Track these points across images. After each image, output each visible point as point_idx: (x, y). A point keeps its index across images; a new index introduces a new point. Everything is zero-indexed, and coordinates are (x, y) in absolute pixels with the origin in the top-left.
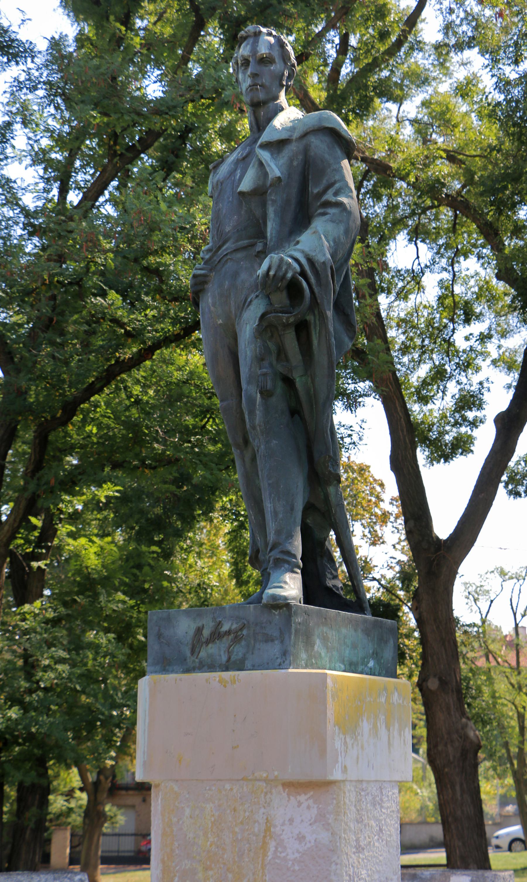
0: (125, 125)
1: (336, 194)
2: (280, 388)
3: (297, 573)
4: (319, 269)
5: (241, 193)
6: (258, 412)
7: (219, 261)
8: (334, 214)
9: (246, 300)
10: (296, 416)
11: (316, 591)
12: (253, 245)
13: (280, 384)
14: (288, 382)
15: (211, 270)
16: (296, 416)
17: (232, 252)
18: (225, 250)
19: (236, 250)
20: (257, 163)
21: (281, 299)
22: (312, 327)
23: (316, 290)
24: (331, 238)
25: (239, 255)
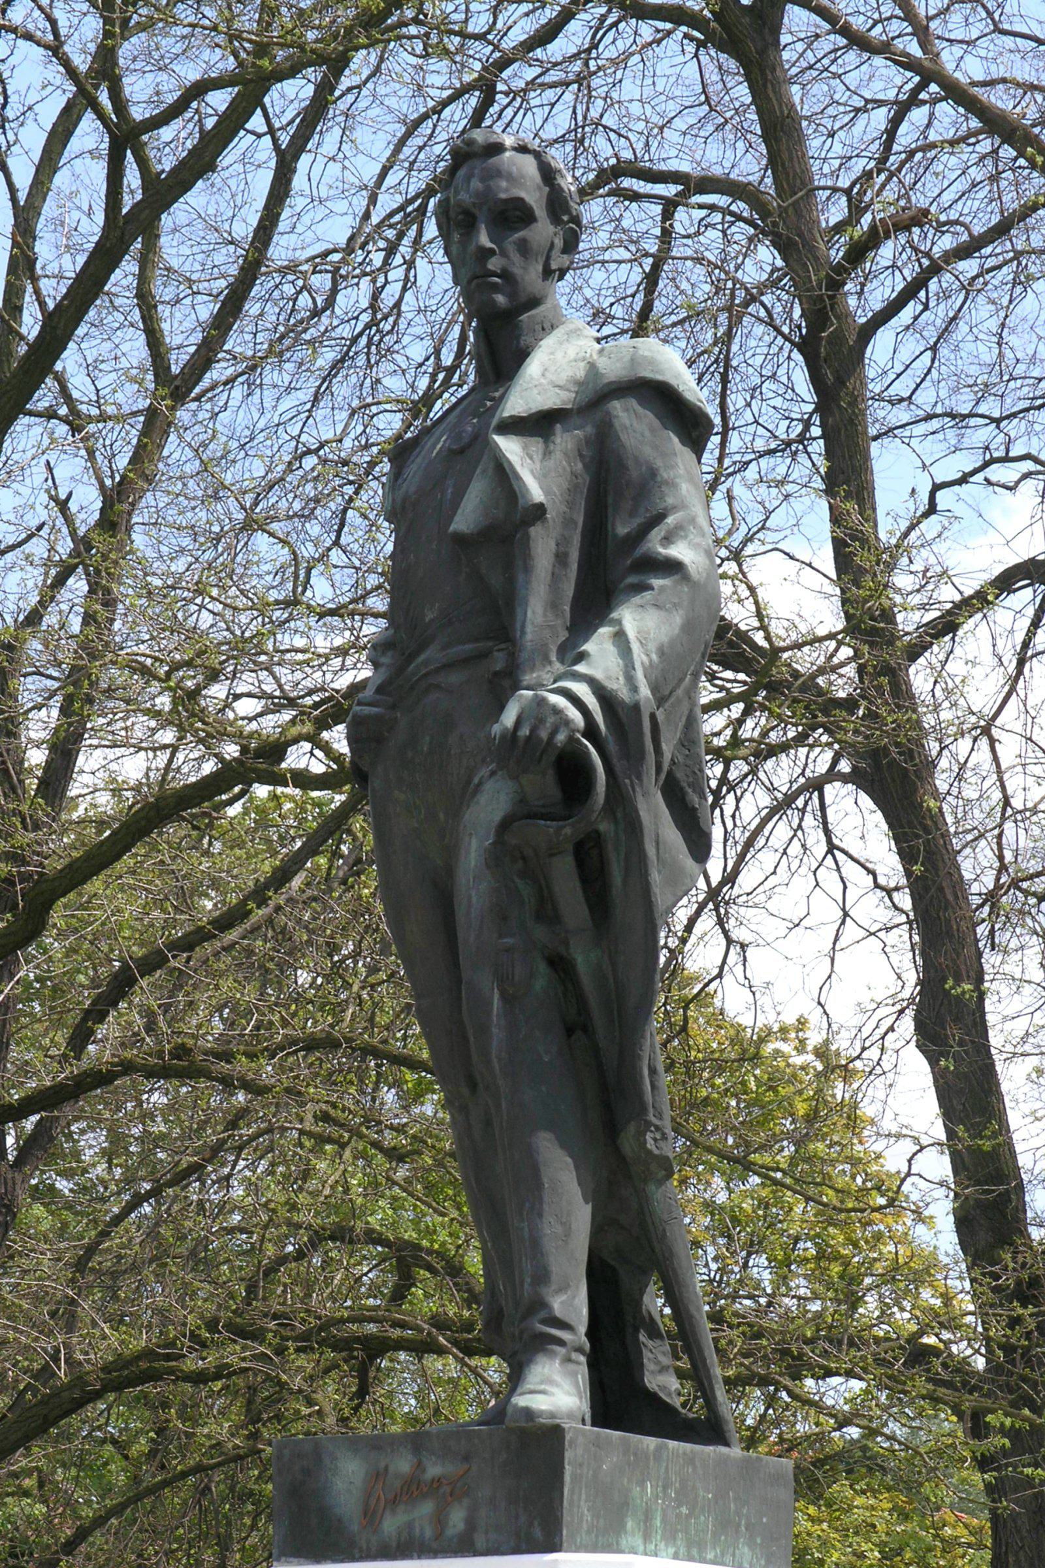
0: (188, 1387)
1: (668, 540)
2: (542, 979)
3: (578, 1363)
4: (625, 720)
5: (460, 540)
6: (495, 1030)
7: (412, 688)
8: (662, 589)
9: (469, 782)
10: (579, 1034)
11: (619, 1400)
12: (484, 655)
13: (542, 967)
14: (560, 965)
15: (393, 707)
16: (579, 1034)
17: (437, 670)
18: (426, 663)
19: (447, 666)
20: (492, 465)
21: (544, 785)
22: (610, 847)
23: (618, 765)
24: (652, 647)
25: (454, 678)
